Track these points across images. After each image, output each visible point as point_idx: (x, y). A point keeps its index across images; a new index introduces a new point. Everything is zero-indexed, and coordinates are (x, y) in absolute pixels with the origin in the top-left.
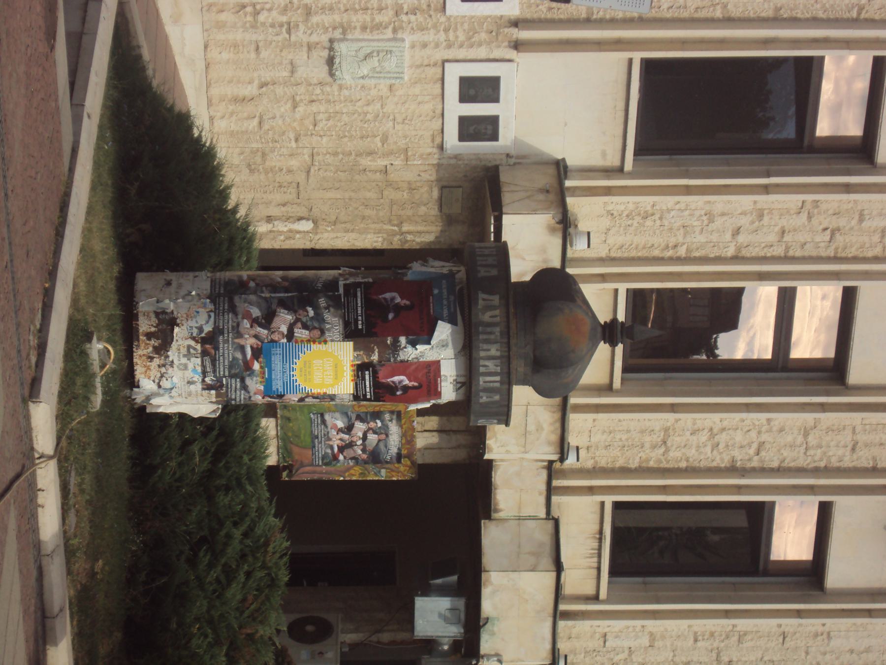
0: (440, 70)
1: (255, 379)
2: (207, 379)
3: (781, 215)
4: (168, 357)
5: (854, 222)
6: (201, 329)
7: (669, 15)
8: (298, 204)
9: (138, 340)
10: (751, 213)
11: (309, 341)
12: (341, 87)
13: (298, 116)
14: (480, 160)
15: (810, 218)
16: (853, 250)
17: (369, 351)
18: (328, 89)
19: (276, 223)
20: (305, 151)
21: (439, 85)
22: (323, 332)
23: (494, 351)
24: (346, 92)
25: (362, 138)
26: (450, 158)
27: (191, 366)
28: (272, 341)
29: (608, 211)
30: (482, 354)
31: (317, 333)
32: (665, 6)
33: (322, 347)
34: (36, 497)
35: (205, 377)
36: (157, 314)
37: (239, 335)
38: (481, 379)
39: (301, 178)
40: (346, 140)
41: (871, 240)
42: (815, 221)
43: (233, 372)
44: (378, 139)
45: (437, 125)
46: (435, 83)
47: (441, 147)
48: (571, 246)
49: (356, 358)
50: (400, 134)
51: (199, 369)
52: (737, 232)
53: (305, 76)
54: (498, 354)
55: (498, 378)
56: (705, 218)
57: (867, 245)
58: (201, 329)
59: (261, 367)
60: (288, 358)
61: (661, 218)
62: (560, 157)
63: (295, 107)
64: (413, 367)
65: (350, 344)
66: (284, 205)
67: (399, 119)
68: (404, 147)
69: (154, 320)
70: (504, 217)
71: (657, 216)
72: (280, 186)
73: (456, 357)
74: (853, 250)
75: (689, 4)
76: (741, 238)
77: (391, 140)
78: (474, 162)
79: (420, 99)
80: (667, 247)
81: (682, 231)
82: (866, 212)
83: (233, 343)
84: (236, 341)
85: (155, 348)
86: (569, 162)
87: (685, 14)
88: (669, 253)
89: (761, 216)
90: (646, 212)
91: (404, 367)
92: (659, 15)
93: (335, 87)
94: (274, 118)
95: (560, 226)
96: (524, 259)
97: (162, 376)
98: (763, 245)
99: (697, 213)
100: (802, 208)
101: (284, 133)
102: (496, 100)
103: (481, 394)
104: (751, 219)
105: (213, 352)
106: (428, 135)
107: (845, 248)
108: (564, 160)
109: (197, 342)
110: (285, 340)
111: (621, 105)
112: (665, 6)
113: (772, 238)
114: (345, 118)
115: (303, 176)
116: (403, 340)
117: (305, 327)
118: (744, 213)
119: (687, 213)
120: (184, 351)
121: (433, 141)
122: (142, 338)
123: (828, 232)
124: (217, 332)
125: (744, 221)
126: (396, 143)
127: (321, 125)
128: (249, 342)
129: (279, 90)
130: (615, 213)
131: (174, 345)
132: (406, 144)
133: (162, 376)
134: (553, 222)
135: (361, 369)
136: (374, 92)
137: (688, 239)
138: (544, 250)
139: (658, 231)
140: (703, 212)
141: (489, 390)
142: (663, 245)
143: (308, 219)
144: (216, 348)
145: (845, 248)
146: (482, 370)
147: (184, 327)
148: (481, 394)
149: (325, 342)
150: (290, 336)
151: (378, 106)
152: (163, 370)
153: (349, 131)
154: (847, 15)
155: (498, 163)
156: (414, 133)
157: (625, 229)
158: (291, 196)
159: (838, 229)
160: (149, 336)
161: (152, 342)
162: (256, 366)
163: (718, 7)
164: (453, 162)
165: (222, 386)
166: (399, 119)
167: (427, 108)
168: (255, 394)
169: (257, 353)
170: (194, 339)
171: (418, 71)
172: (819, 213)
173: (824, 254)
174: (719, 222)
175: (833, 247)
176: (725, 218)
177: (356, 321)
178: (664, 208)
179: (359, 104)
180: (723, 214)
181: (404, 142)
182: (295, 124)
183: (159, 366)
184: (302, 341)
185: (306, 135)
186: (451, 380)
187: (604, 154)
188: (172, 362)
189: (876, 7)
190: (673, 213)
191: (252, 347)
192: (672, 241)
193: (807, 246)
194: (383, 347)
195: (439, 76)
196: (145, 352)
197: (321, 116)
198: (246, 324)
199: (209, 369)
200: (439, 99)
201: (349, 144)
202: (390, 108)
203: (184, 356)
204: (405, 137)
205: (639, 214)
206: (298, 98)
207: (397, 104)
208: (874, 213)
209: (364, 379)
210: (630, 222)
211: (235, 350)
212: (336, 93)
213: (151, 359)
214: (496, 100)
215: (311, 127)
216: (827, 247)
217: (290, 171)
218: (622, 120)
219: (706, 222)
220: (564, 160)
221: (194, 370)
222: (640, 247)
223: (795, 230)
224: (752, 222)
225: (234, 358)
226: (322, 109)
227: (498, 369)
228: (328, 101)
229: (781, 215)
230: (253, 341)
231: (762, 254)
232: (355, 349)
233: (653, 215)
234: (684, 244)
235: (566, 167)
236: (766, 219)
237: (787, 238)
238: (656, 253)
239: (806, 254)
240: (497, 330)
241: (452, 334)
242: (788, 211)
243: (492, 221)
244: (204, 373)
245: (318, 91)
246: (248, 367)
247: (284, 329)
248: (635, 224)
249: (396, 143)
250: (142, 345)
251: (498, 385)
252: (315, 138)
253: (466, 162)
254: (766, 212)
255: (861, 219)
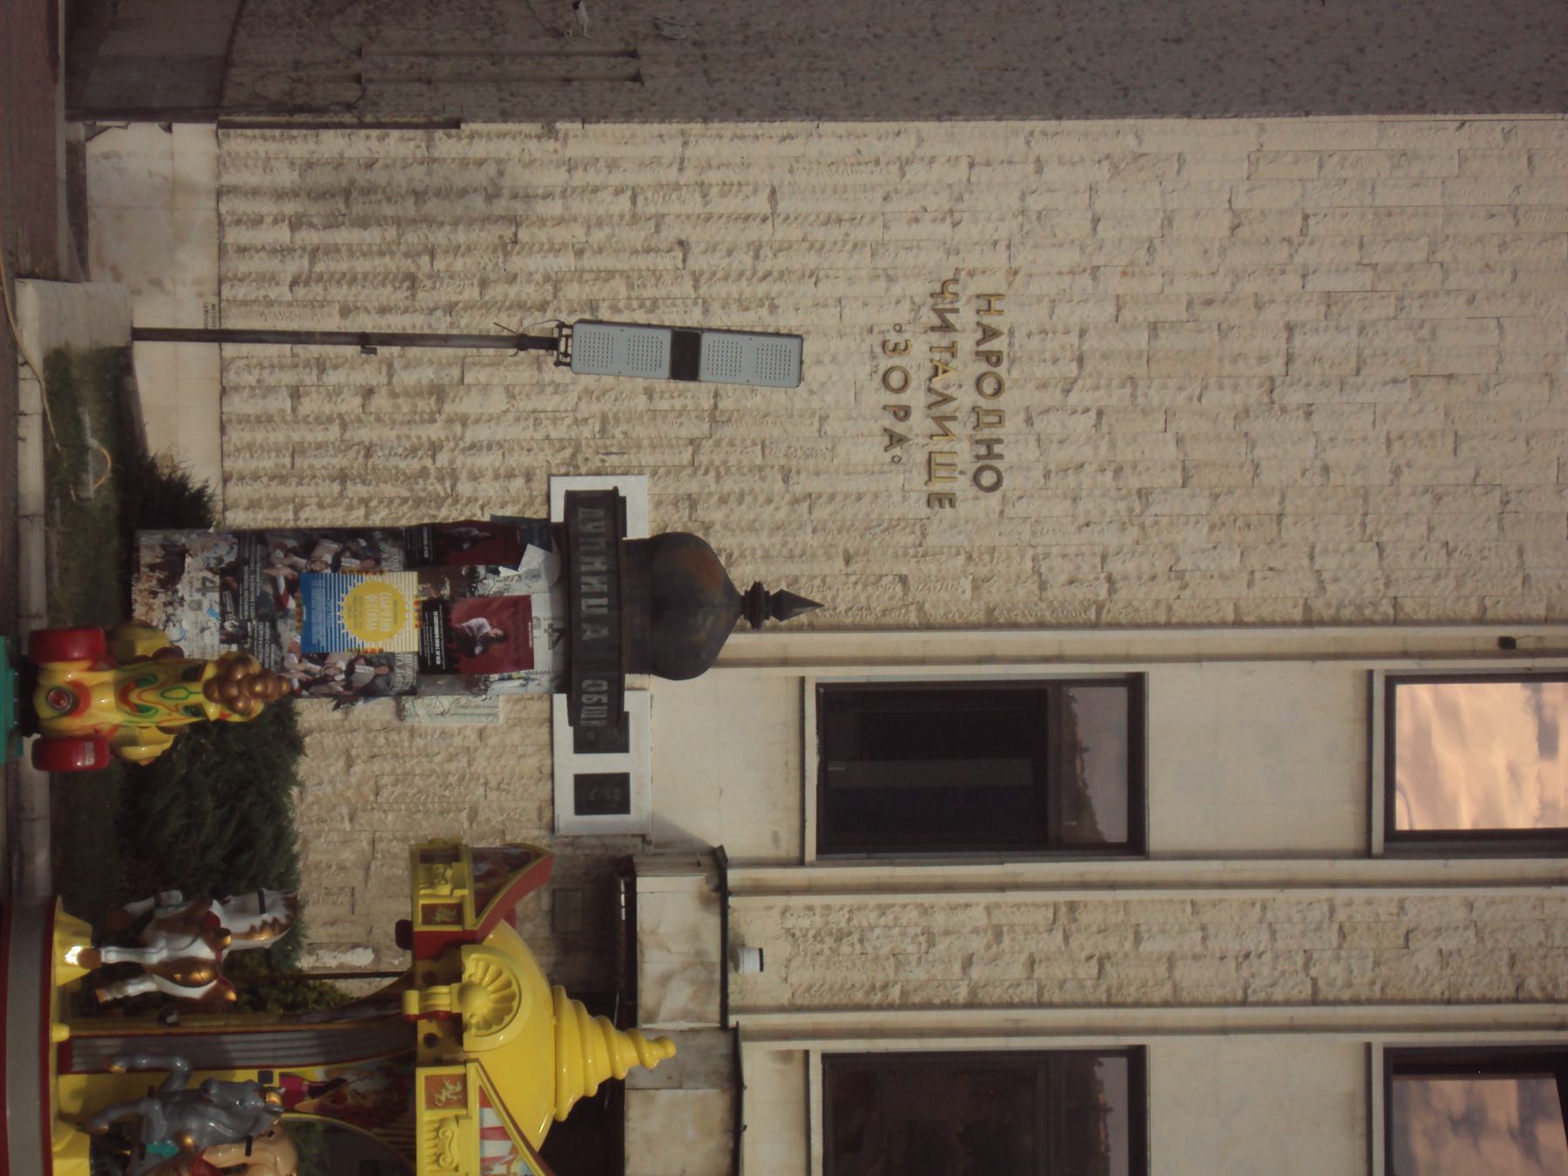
0: (546, 705)
1: (290, 621)
2: (227, 624)
3: (1027, 933)
4: (176, 591)
5: (1128, 945)
6: (220, 560)
7: (848, 621)
8: (353, 923)
9: (138, 571)
10: (985, 930)
11: (360, 572)
12: (413, 733)
13: (353, 780)
14: (604, 846)
15: (1066, 938)
16: (1133, 989)
17: (439, 585)
18: (395, 737)
19: (321, 952)
20: (363, 836)
21: (545, 730)
22: (378, 562)
23: (599, 564)
24: (420, 742)
25: (442, 813)
26: (565, 845)
27: (206, 604)
28: (313, 571)
29: (788, 930)
30: (584, 568)
31: (370, 563)
32: (842, 608)
33: (377, 579)
34: (17, 422)
35: (224, 620)
36: (163, 547)
37: (270, 565)
38: (584, 602)
39: (356, 878)
40: (419, 816)
41: (1154, 973)
42: (1074, 944)
43: (262, 611)
44: (464, 814)
45: (543, 791)
46: (541, 724)
47: (552, 828)
48: (737, 968)
49: (422, 592)
50: (495, 805)
51: (217, 609)
52: (968, 963)
53: (363, 718)
54: (604, 568)
55: (604, 601)
56: (922, 939)
57: (1151, 983)
58: (220, 560)
59: (299, 606)
60: (333, 593)
61: (861, 941)
62: (716, 845)
63: (350, 764)
64: (495, 605)
65: (414, 575)
66: (333, 924)
67: (493, 783)
68: (499, 827)
69: (160, 552)
70: (639, 880)
71: (856, 937)
72: (328, 894)
73: (551, 589)
74: (1133, 989)
75: (874, 604)
76: (976, 973)
77: (482, 817)
78: (598, 852)
79: (520, 750)
80: (873, 988)
81: (892, 960)
82: (1143, 928)
83: (262, 574)
84: (267, 571)
85: (159, 580)
86: (729, 853)
87: (870, 619)
88: (877, 998)
89: (998, 935)
90: (840, 930)
91: (486, 606)
92: (834, 621)
93: (405, 735)
94: (320, 784)
95: (715, 895)
96: (669, 951)
97: (168, 620)
98: (1006, 984)
99: (911, 931)
100: (1054, 921)
101: (334, 807)
102: (623, 747)
103: (585, 626)
104: (985, 941)
105: (235, 585)
106: (532, 807)
107: (1120, 988)
108: (721, 848)
109: (215, 573)
110: (329, 571)
111: (794, 761)
112: (842, 608)
113: (1017, 971)
114: (418, 781)
115: (360, 875)
116: (481, 570)
117: (355, 556)
118: (976, 931)
119: (896, 931)
120: (198, 585)
121: (540, 817)
122: (143, 569)
123: (1094, 962)
124: (241, 562)
125: (977, 944)
126: (488, 820)
127: (385, 793)
128: (282, 574)
129: (328, 740)
130: (798, 933)
131: (185, 577)
132: (503, 823)
133: (168, 620)
134: (706, 888)
135: (427, 608)
136: (457, 740)
137: (902, 976)
138: (695, 935)
139: (858, 963)
140: (919, 930)
141: (595, 620)
142: (867, 985)
143: (366, 947)
144: (240, 580)
145: (1120, 988)
146: (584, 588)
147: (199, 558)
148: (585, 626)
149: (382, 572)
150: (336, 566)
151: (464, 761)
152: (170, 610)
153: (424, 804)
154: (1082, 618)
155: (630, 852)
156: (513, 805)
157: (812, 959)
158: (342, 910)
159: (1108, 957)
160: (153, 567)
161: (157, 574)
162: (292, 604)
163: (912, 608)
164: (568, 851)
165: (246, 636)
166: (493, 783)
167: (531, 763)
168: (290, 651)
169: (292, 586)
170: (210, 569)
171: (517, 707)
172: (1078, 930)
173: (1091, 998)
174: (942, 945)
175: (1104, 987)
176: (950, 938)
177: (422, 551)
178: (865, 924)
179: (437, 759)
180: (947, 933)
181: (500, 819)
182: (349, 793)
183: (165, 605)
184: (351, 572)
185: (365, 810)
186: (545, 624)
187: (776, 838)
188: (182, 598)
189: (1120, 605)
190: (877, 931)
191: (286, 579)
192: (880, 978)
193: (1068, 986)
194: (456, 580)
195: (546, 715)
196: (147, 586)
197: (386, 780)
198: (279, 554)
199: (229, 609)
200: (546, 751)
201: (424, 824)
202: (480, 765)
203: (198, 590)
204: (502, 811)
205: (831, 934)
206: (354, 753)
207: (488, 759)
208: (1155, 929)
209: (432, 624)
210: (818, 947)
211: (264, 581)
212: (406, 744)
213: (154, 594)
214: (623, 747)
215: (372, 798)
216: (1096, 987)
217: (342, 868)
218: (797, 783)
219: (924, 946)
220: (721, 848)
221: (211, 610)
222: (837, 987)
223: (1048, 959)
224: (988, 947)
225: (264, 594)
226: (387, 768)
227: (605, 588)
228: (396, 756)
229: (1027, 933)
230: (287, 571)
231: (1006, 998)
232: (420, 581)
233: (850, 934)
234: (896, 983)
235: (725, 859)
236: (1006, 940)
237: (1039, 972)
238: (859, 996)
239: (1068, 998)
240: (602, 541)
241: (546, 560)
242: (1036, 928)
243: (623, 888)
244: (223, 615)
245: (381, 741)
246: (280, 603)
247: (328, 558)
248: (827, 952)
249: (488, 820)
250: (144, 578)
251: (605, 611)
252: (377, 815)
253: (587, 852)
254: (1005, 929)
255: (1138, 940)
